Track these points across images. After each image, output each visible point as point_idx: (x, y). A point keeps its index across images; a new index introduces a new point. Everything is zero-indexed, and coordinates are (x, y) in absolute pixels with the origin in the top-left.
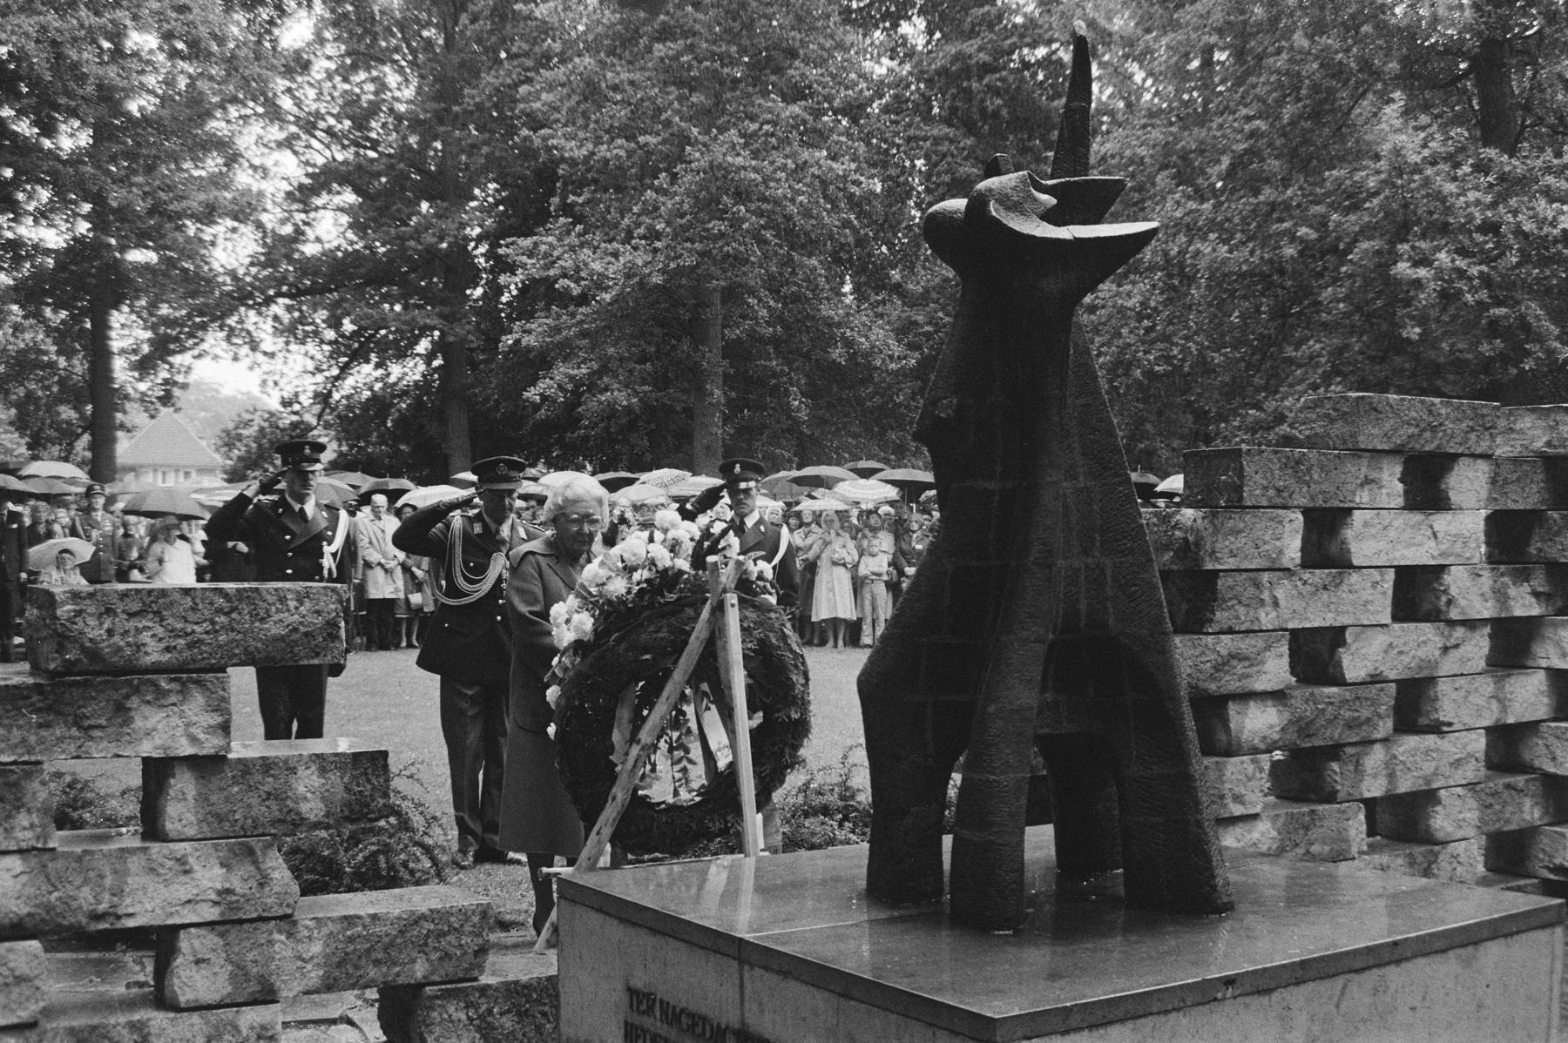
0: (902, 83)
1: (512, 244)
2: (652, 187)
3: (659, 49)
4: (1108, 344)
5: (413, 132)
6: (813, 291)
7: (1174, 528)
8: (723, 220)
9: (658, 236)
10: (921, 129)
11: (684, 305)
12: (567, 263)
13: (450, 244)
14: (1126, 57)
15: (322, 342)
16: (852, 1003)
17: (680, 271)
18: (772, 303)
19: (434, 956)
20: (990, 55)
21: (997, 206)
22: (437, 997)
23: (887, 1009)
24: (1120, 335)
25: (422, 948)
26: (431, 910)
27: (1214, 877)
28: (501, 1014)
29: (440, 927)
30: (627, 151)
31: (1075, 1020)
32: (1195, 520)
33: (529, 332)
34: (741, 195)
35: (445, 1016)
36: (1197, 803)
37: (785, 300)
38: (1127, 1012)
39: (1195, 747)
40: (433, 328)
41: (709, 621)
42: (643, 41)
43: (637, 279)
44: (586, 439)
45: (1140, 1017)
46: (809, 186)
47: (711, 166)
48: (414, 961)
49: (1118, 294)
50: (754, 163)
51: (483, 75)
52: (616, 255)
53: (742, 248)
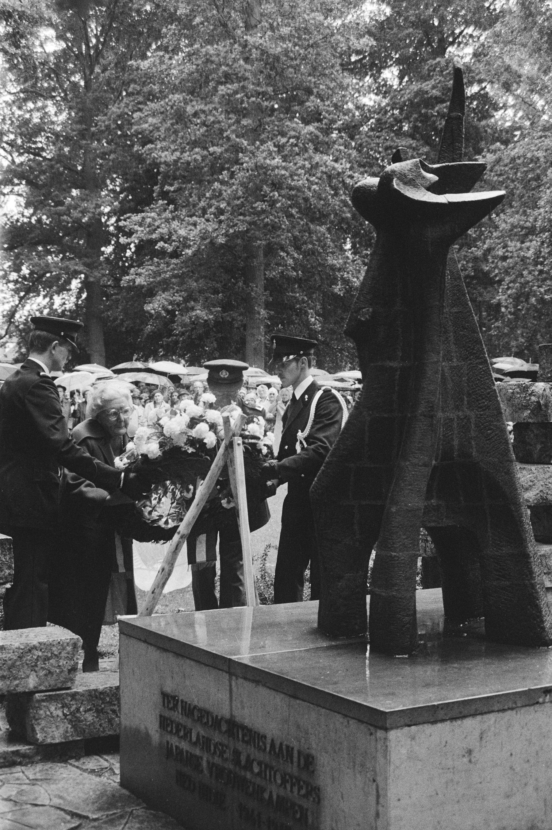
0: (382, 111)
1: (129, 218)
2: (218, 180)
3: (223, 90)
4: (514, 281)
5: (66, 145)
6: (322, 247)
7: (530, 395)
8: (264, 201)
9: (221, 212)
10: (394, 142)
11: (240, 257)
12: (164, 230)
13: (90, 219)
14: (532, 91)
15: (9, 281)
16: (298, 701)
17: (237, 235)
18: (296, 255)
19: (42, 673)
20: (440, 91)
21: (398, 181)
22: (43, 701)
23: (318, 706)
24: (522, 276)
25: (33, 668)
26: (39, 643)
27: (543, 622)
28: (85, 712)
29: (46, 654)
30: (202, 157)
31: (441, 714)
32: (544, 390)
33: (139, 275)
34: (276, 186)
35: (48, 713)
36: (531, 572)
37: (306, 254)
38: (476, 710)
39: (530, 536)
40: (81, 273)
41: (224, 455)
42: (212, 84)
43: (208, 241)
44: (176, 342)
45: (486, 713)
46: (320, 179)
47: (256, 166)
48: (28, 677)
49: (521, 249)
50: (284, 164)
51: (109, 107)
52: (195, 225)
53: (276, 220)
